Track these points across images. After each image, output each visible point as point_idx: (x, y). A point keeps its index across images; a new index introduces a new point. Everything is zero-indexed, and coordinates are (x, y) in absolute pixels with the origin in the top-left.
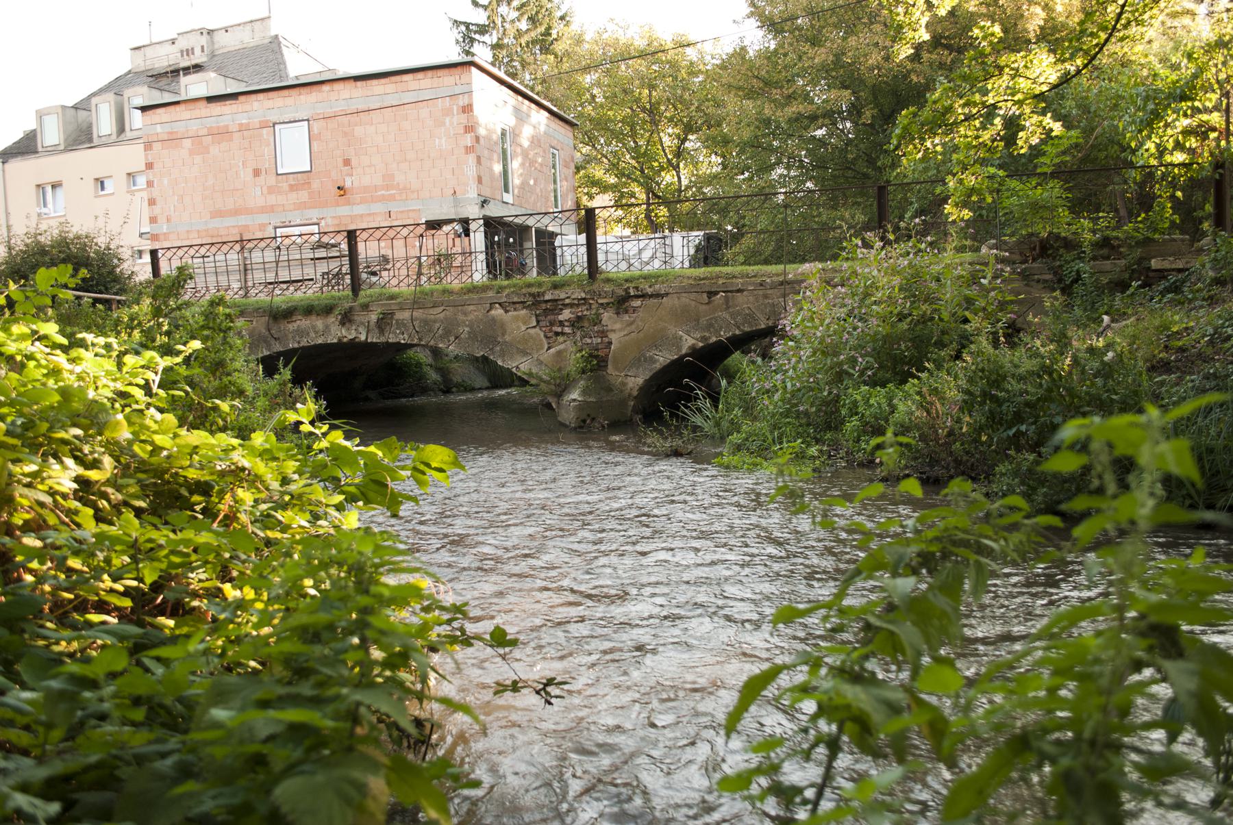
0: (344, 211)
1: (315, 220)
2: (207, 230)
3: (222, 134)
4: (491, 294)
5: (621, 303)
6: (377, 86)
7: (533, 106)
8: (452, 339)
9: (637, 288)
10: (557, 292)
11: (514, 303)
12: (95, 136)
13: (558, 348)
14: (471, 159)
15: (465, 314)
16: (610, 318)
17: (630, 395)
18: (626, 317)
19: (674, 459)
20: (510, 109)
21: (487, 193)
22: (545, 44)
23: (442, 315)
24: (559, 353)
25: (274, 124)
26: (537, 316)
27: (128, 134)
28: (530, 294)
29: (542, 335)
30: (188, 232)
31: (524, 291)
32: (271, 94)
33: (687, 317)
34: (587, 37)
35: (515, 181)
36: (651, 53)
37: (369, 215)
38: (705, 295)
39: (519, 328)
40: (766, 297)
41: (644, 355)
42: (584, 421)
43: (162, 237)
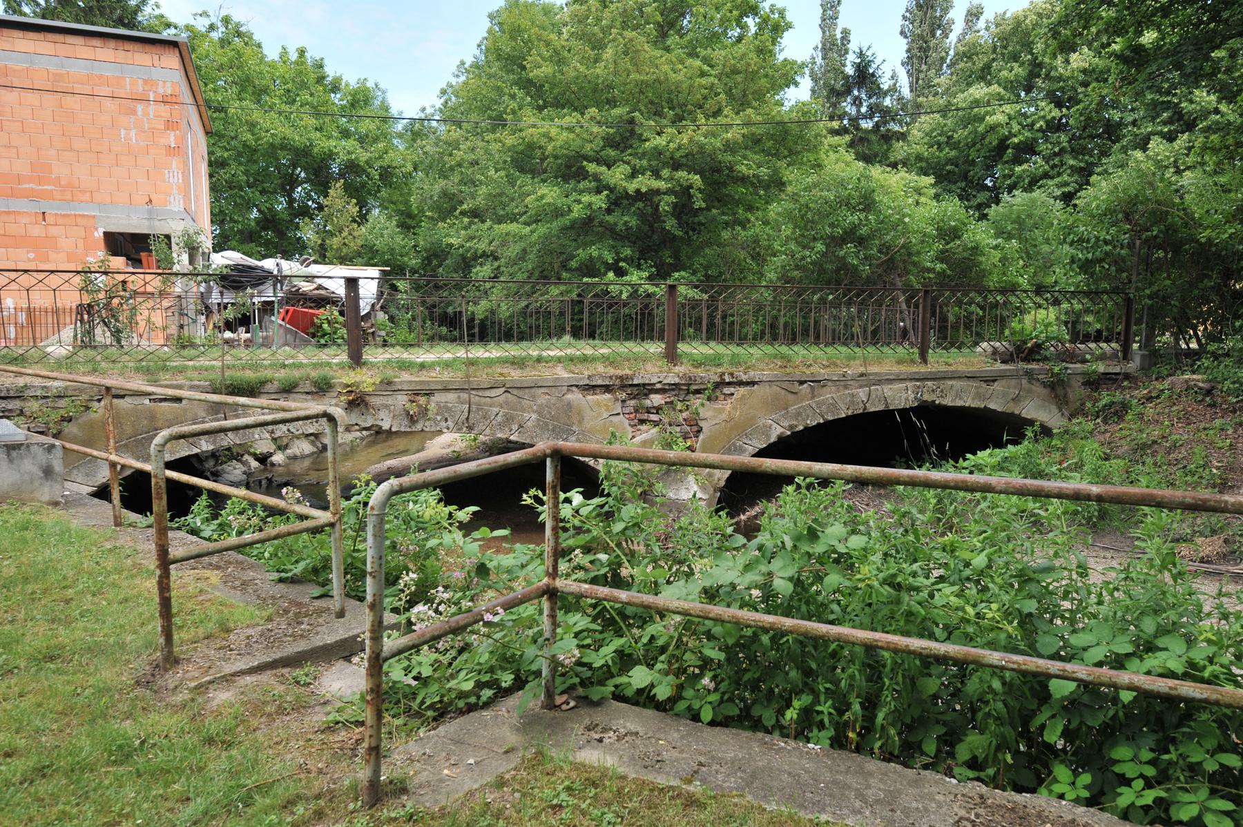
8: (515, 427)
9: (732, 374)
23: (501, 399)
41: (734, 444)
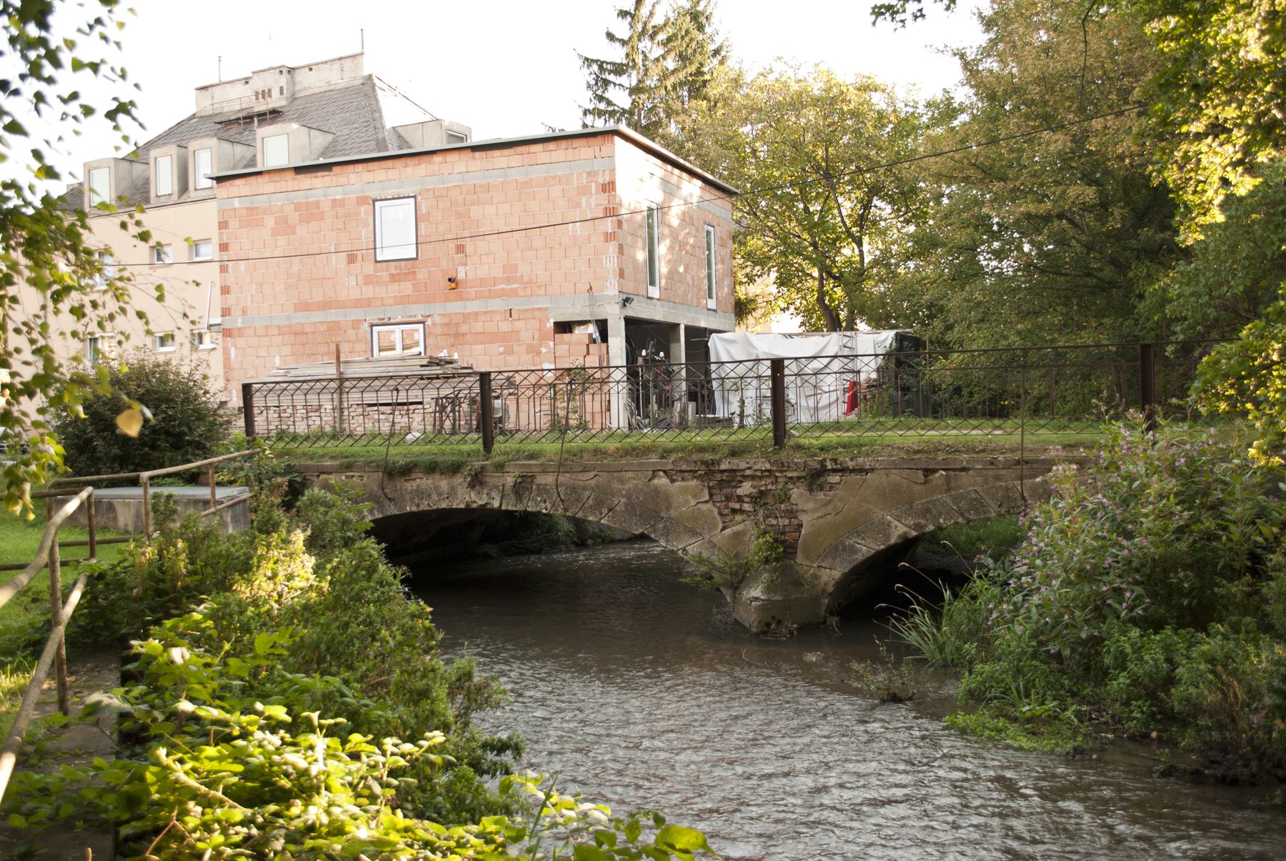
0: (455, 307)
1: (419, 318)
2: (289, 326)
3: (311, 212)
4: (654, 459)
5: (815, 478)
6: (499, 158)
7: (684, 175)
8: (605, 511)
9: (835, 460)
10: (735, 461)
11: (682, 471)
12: (152, 195)
13: (736, 528)
14: (612, 248)
15: (622, 482)
16: (801, 495)
17: (824, 591)
18: (821, 496)
19: (895, 706)
20: (656, 181)
21: (630, 287)
22: (696, 87)
24: (737, 535)
25: (374, 201)
26: (710, 488)
27: (192, 194)
28: (703, 462)
29: (716, 511)
30: (267, 327)
31: (695, 457)
32: (371, 165)
33: (897, 499)
34: (748, 78)
35: (662, 268)
36: (829, 102)
37: (486, 313)
38: (920, 473)
39: (687, 501)
40: (998, 478)
41: (842, 543)
42: (768, 625)
43: (235, 333)
